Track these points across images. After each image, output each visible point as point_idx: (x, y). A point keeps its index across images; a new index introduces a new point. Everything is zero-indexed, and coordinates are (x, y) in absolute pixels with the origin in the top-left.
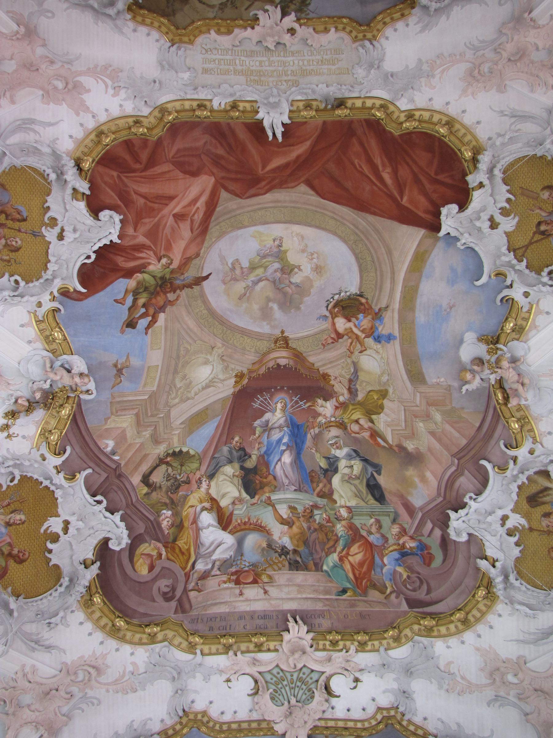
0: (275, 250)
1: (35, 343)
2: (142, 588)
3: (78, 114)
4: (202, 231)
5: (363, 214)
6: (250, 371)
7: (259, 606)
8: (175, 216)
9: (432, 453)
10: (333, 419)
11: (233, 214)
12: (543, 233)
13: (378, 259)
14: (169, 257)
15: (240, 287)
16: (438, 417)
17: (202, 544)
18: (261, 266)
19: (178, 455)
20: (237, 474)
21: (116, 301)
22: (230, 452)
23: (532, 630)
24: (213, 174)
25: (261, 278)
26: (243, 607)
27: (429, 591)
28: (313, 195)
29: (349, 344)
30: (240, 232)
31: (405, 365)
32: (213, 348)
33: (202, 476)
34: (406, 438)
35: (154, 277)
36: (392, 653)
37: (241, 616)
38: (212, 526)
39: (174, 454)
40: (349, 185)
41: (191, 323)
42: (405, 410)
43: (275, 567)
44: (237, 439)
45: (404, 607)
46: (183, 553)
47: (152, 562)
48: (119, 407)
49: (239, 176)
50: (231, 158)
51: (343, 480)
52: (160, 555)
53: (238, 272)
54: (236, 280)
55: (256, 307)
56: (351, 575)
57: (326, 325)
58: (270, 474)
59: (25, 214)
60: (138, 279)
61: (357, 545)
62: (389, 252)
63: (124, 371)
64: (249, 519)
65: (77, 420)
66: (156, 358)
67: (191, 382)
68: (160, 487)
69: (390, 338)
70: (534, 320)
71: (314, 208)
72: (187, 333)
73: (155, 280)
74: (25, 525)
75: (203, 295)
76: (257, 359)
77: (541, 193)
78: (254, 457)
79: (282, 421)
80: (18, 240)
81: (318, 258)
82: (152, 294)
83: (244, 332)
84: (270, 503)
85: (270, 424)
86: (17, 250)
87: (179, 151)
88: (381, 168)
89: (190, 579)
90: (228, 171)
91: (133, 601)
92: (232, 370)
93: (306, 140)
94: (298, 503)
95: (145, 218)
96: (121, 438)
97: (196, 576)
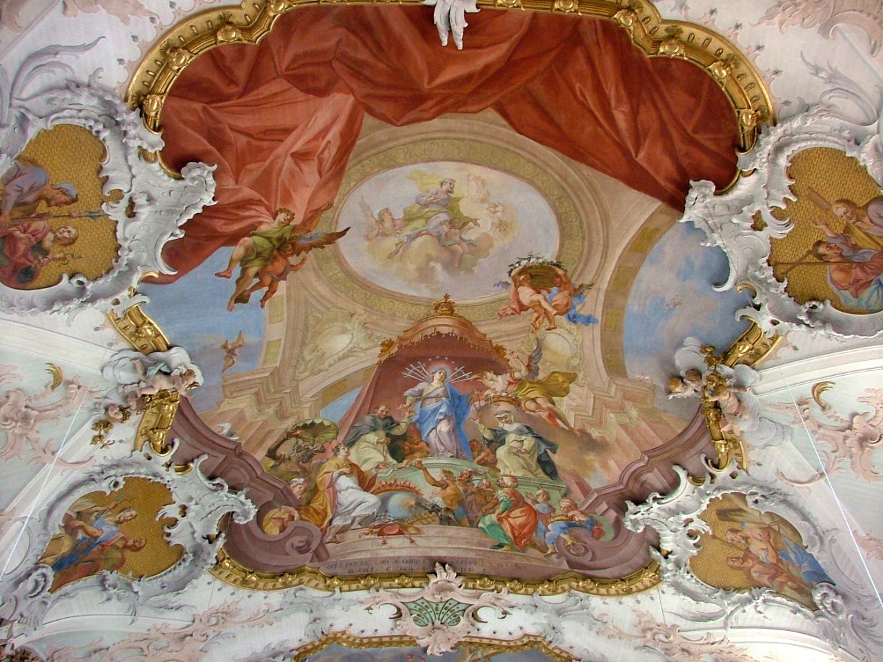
0: (443, 196)
1: (117, 344)
2: (274, 546)
3: (126, 21)
4: (337, 171)
5: (577, 163)
6: (401, 339)
7: (404, 553)
8: (293, 155)
9: (619, 444)
10: (504, 394)
11: (383, 147)
12: (820, 256)
13: (589, 227)
14: (287, 211)
15: (390, 243)
16: (634, 413)
17: (340, 504)
18: (422, 217)
19: (312, 428)
20: (382, 441)
21: (218, 275)
22: (374, 421)
23: (692, 611)
24: (352, 91)
25: (420, 232)
26: (385, 553)
27: (593, 559)
28: (504, 126)
29: (534, 319)
30: (391, 173)
31: (604, 353)
32: (352, 315)
33: (340, 445)
34: (592, 425)
35: (268, 238)
36: (546, 598)
37: (385, 561)
38: (352, 488)
39: (305, 427)
40: (561, 118)
41: (322, 289)
42: (595, 397)
43: (424, 521)
44: (382, 408)
45: (565, 566)
46: (318, 513)
47: (283, 523)
48: (233, 388)
49: (393, 92)
50: (381, 66)
51: (510, 452)
52: (292, 518)
53: (388, 224)
54: (384, 235)
55: (411, 267)
56: (509, 534)
57: (507, 293)
58: (422, 441)
59: (73, 193)
60: (246, 244)
61: (519, 510)
62: (606, 220)
63: (237, 351)
64: (395, 481)
65: (185, 411)
66: (277, 331)
67: (323, 355)
68: (289, 459)
69: (589, 320)
70: (776, 350)
71: (505, 145)
72: (318, 300)
73: (271, 242)
74: (137, 519)
75: (338, 257)
76: (411, 326)
77: (834, 207)
78: (403, 425)
79: (440, 391)
80: (70, 229)
81: (503, 211)
82: (267, 260)
83: (393, 296)
84: (420, 466)
85: (424, 394)
86: (72, 241)
87: (296, 58)
88: (613, 103)
89: (328, 533)
90: (376, 85)
91: (263, 558)
92: (378, 338)
93: (502, 41)
94: (454, 468)
95: (251, 162)
96: (240, 418)
97: (333, 530)
